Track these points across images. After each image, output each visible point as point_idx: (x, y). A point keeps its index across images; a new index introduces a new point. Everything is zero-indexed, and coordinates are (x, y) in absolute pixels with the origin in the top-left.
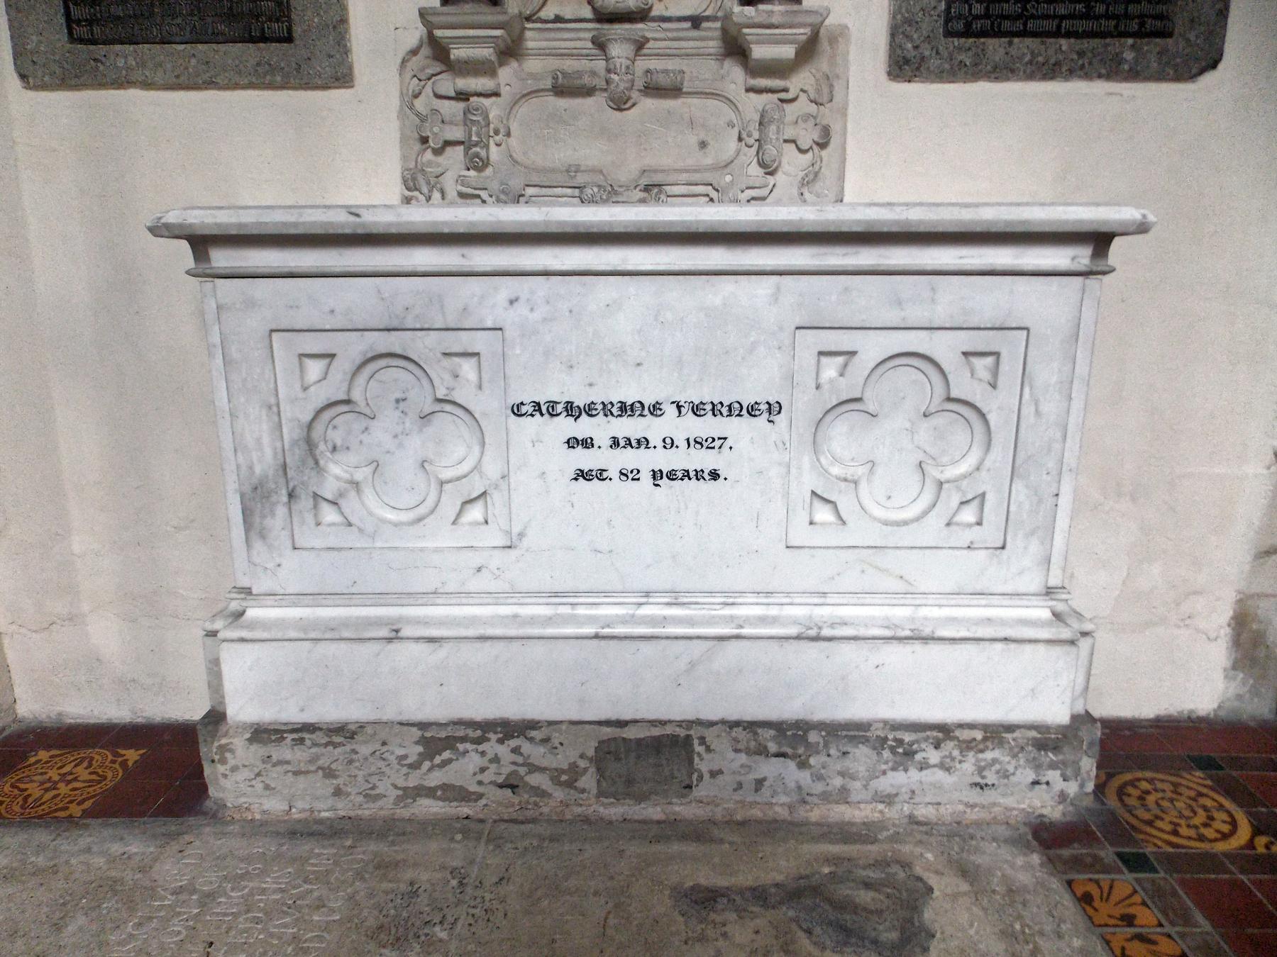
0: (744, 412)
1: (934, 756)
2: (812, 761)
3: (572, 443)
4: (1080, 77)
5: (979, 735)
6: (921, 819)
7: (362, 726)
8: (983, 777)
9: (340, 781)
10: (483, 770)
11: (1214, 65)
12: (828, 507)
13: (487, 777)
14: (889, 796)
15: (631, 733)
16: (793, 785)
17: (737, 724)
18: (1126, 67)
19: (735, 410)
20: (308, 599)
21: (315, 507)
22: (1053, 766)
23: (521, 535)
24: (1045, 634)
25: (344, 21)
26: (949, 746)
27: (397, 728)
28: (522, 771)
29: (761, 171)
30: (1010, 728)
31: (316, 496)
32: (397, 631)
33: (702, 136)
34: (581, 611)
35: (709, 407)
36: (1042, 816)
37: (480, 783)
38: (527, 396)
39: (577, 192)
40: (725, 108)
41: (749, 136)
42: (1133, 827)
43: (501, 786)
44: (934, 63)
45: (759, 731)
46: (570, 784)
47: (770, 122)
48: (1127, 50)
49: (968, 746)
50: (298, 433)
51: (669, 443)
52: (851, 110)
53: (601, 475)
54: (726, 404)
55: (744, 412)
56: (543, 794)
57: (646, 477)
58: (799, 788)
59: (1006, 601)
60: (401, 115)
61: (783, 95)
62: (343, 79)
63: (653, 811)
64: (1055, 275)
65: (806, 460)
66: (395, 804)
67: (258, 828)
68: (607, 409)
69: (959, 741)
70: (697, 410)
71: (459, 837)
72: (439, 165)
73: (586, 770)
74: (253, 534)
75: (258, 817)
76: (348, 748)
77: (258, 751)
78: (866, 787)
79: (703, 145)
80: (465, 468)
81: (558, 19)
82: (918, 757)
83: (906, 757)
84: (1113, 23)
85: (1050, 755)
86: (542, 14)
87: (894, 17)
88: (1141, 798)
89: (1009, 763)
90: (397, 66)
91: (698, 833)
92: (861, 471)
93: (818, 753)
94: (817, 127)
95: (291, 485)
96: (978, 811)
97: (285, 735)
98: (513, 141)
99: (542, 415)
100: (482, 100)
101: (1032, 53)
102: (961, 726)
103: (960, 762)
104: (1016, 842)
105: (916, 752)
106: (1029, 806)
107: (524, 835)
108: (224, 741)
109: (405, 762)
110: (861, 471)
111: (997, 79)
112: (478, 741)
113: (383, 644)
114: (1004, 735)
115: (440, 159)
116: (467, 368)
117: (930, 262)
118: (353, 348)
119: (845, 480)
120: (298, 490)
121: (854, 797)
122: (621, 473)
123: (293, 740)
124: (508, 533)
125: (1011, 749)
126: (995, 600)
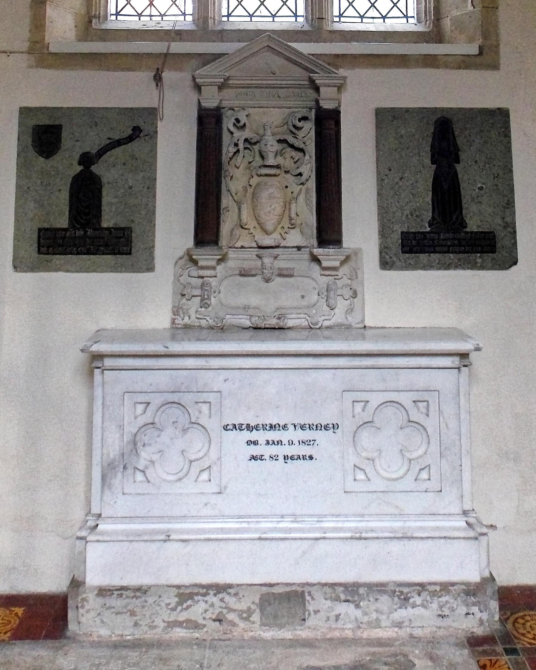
0: (323, 428)
1: (418, 600)
2: (362, 604)
3: (249, 443)
4: (459, 269)
5: (438, 588)
6: (416, 636)
7: (150, 587)
8: (442, 611)
9: (138, 618)
10: (206, 611)
11: (515, 263)
12: (362, 472)
13: (208, 615)
14: (400, 623)
15: (276, 590)
16: (353, 618)
17: (326, 584)
18: (479, 265)
19: (318, 427)
20: (127, 520)
21: (134, 473)
22: (474, 604)
23: (226, 487)
24: (462, 535)
25: (153, 246)
26: (424, 594)
27: (166, 589)
28: (225, 611)
29: (328, 309)
30: (453, 584)
31: (136, 468)
32: (169, 536)
33: (303, 294)
34: (252, 525)
35: (308, 426)
36: (472, 633)
37: (204, 618)
38: (230, 421)
39: (248, 317)
40: (311, 281)
41: (322, 294)
42: (515, 637)
43: (214, 620)
44: (398, 263)
45: (336, 588)
46: (247, 619)
47: (331, 290)
48: (478, 258)
49: (433, 594)
50: (131, 437)
51: (291, 443)
52: (365, 282)
53: (261, 458)
54: (315, 424)
55: (323, 428)
56: (234, 624)
57: (281, 458)
58: (356, 619)
59: (446, 518)
60: (174, 283)
61: (336, 277)
62: (150, 268)
63: (286, 634)
64: (446, 368)
65: (351, 450)
66: (163, 631)
67: (98, 644)
68: (264, 427)
69: (429, 591)
70: (302, 427)
71: (195, 647)
72: (188, 305)
73: (255, 611)
74: (106, 488)
75: (96, 639)
76: (143, 599)
77: (100, 601)
78: (388, 618)
79: (303, 297)
80: (201, 454)
81: (242, 247)
82: (411, 601)
83: (405, 600)
84: (471, 248)
85: (472, 598)
86: (236, 245)
87: (381, 246)
88: (524, 624)
89: (454, 603)
90: (174, 264)
91: (308, 644)
92: (375, 454)
93: (364, 599)
94: (352, 290)
95: (125, 462)
96: (443, 631)
97: (114, 592)
98: (221, 295)
99: (236, 430)
100: (209, 278)
101: (439, 260)
102: (430, 584)
103: (431, 603)
104: (459, 645)
105: (409, 598)
106: (467, 627)
107: (227, 646)
108: (84, 596)
109: (170, 607)
110: (375, 454)
111: (425, 270)
112: (204, 595)
113: (162, 542)
114: (450, 588)
115: (189, 302)
116: (205, 408)
117: (395, 363)
118: (157, 400)
119: (369, 459)
120: (127, 465)
121: (383, 624)
122: (271, 457)
123: (118, 595)
124: (220, 486)
125: (454, 595)
126: (440, 517)
